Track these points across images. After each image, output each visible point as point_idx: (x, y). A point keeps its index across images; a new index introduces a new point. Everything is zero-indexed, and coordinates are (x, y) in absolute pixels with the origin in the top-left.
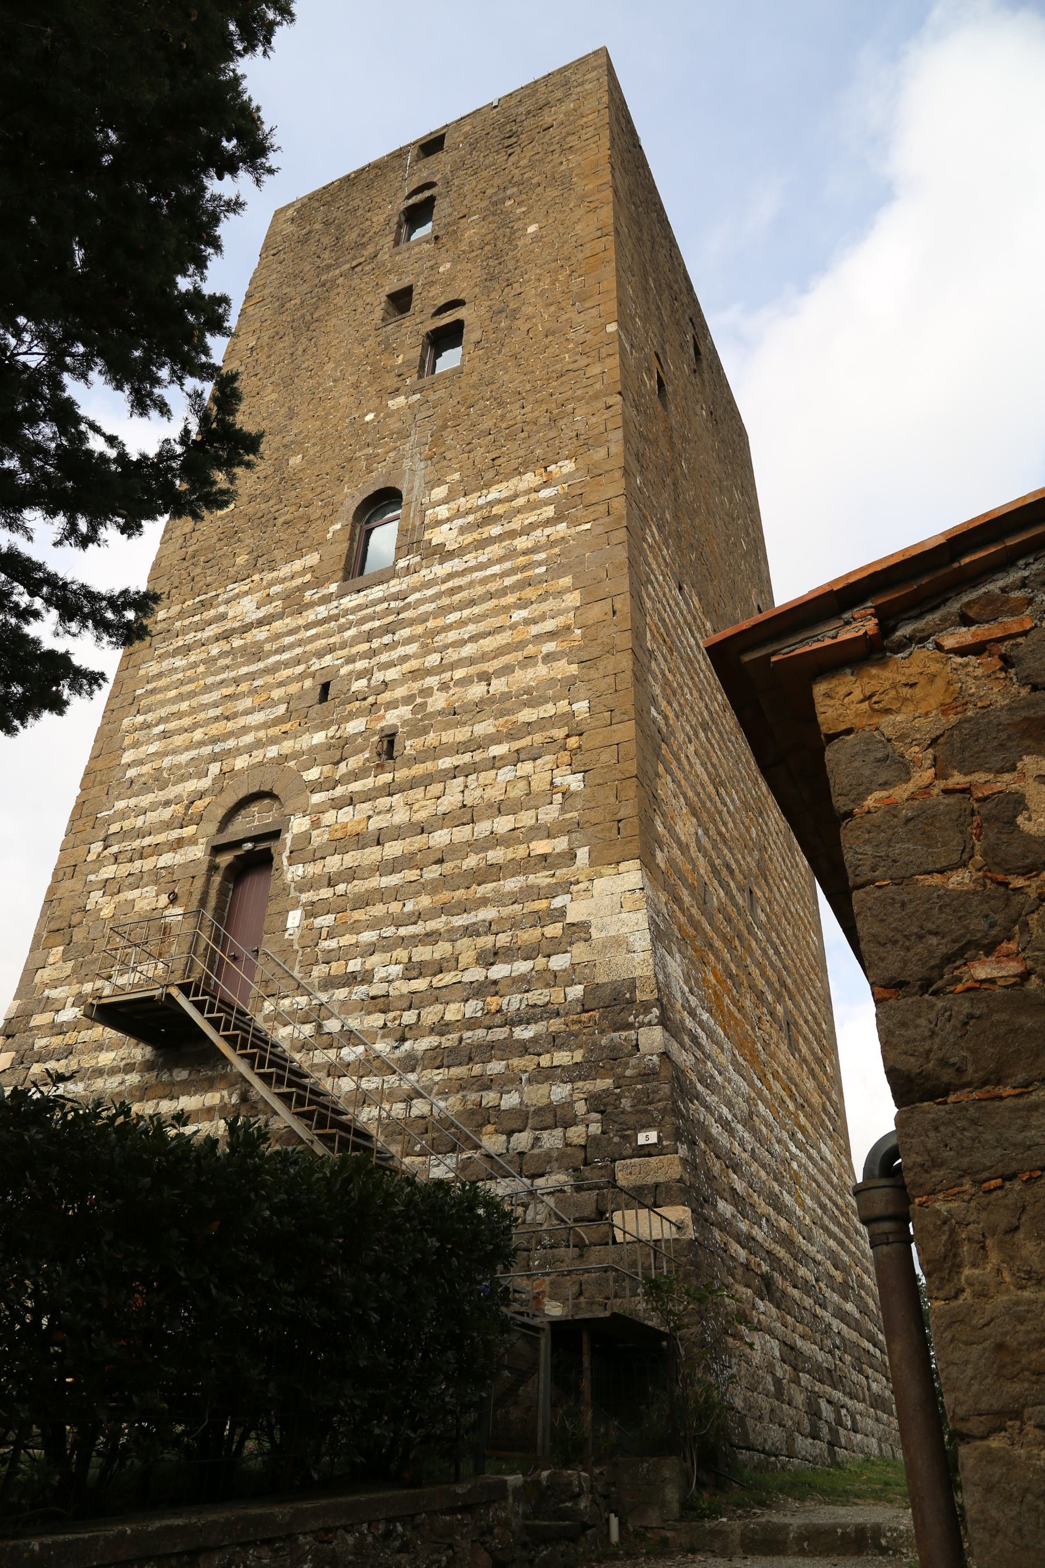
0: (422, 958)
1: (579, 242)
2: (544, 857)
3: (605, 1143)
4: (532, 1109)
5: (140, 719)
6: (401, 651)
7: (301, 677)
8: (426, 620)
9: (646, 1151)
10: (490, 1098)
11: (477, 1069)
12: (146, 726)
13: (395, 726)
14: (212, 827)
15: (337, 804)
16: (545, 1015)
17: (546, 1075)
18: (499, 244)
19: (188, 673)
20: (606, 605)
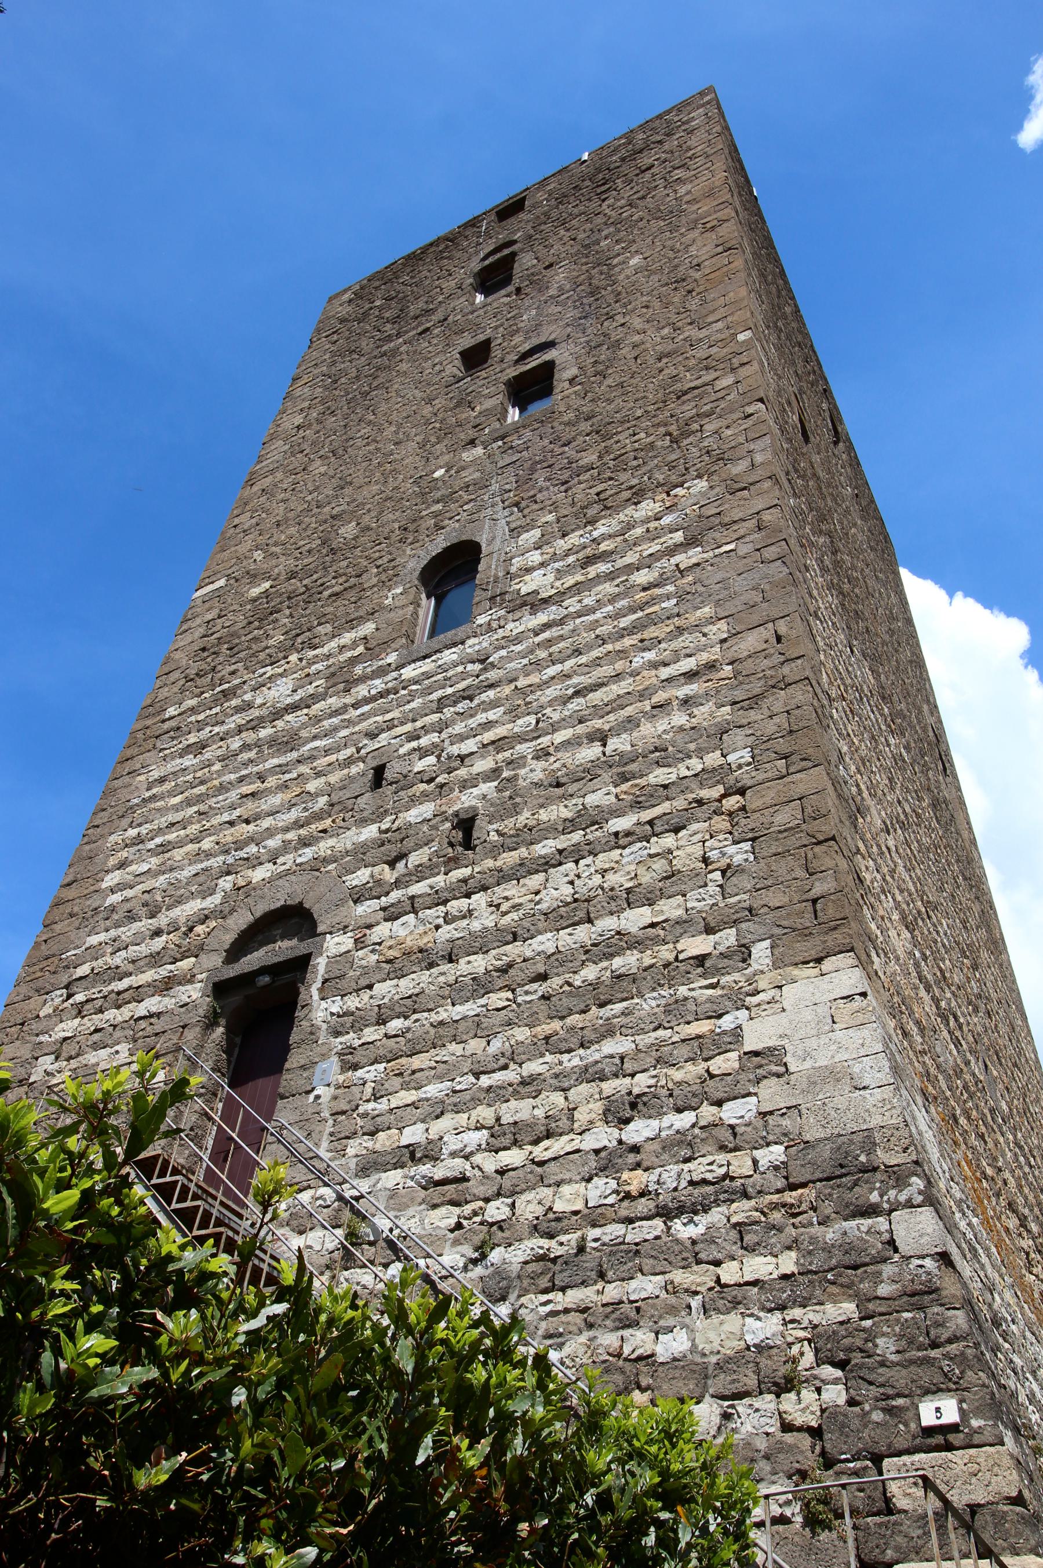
0: (517, 1118)
1: (695, 262)
2: (701, 960)
3: (856, 1423)
4: (713, 1359)
5: (132, 832)
6: (481, 718)
7: (349, 762)
8: (515, 680)
9: (941, 1438)
10: (639, 1340)
11: (613, 1292)
12: (139, 840)
13: (474, 808)
14: (215, 960)
15: (391, 915)
16: (722, 1197)
17: (727, 1298)
18: (594, 282)
19: (199, 774)
20: (767, 632)
